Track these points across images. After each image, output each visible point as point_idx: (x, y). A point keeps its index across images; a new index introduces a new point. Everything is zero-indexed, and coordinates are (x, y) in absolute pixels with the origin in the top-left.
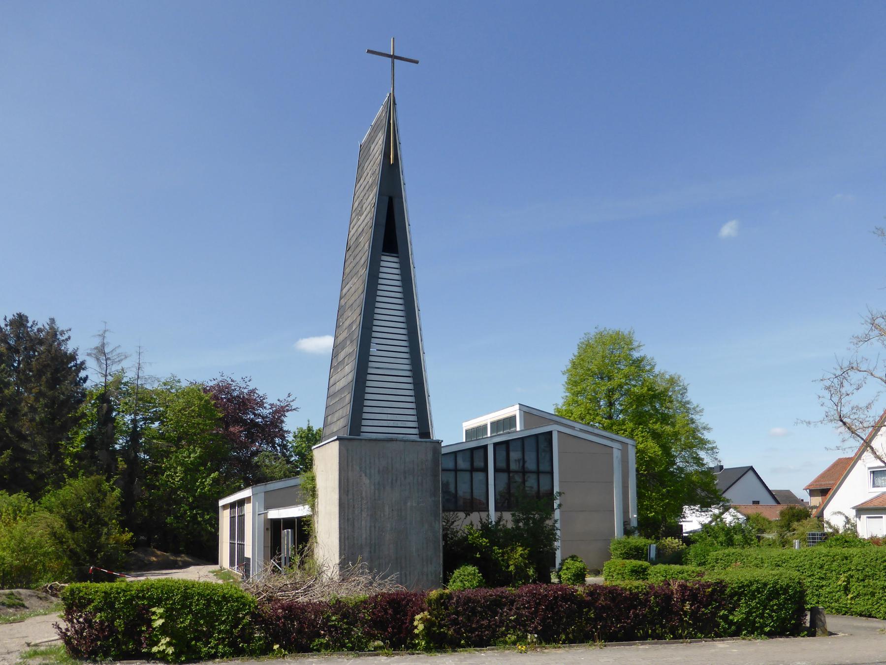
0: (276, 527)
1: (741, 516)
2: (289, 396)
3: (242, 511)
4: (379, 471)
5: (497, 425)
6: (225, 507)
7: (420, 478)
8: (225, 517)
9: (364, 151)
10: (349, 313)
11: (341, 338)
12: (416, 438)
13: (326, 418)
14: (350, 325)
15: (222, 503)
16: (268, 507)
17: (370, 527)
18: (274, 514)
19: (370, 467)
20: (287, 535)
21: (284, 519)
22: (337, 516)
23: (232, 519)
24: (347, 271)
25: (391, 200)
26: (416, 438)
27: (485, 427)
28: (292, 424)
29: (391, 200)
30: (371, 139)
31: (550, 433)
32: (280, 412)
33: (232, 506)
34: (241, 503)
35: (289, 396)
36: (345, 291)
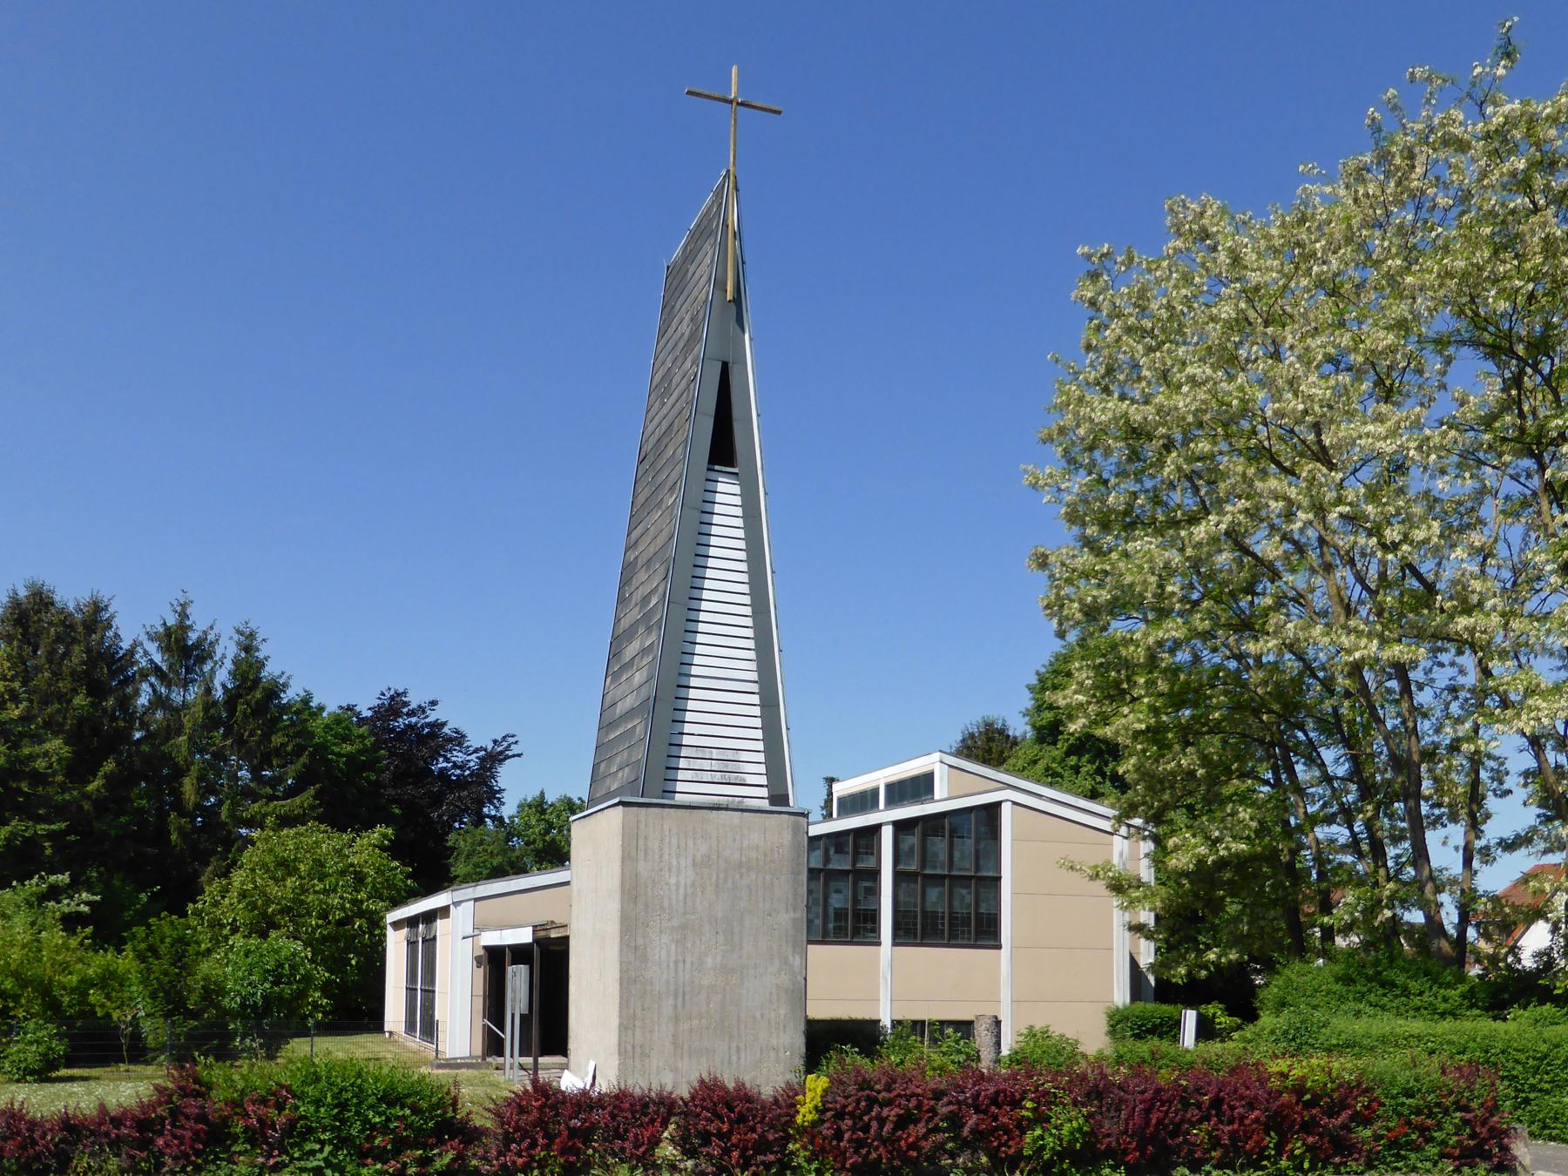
0: (495, 961)
1: (666, 827)
2: (1042, 562)
3: (429, 929)
4: (694, 864)
5: (901, 791)
6: (397, 925)
7: (768, 877)
8: (396, 945)
9: (677, 278)
10: (642, 576)
11: (625, 623)
12: (765, 804)
13: (595, 767)
14: (646, 599)
15: (392, 917)
16: (479, 928)
17: (676, 962)
18: (492, 938)
19: (678, 856)
20: (518, 979)
21: (510, 947)
22: (617, 940)
23: (412, 944)
24: (641, 498)
25: (725, 367)
26: (765, 804)
27: (875, 791)
28: (516, 788)
29: (725, 367)
30: (690, 255)
31: (997, 806)
32: (493, 758)
33: (412, 922)
34: (430, 917)
35: (1042, 562)
36: (634, 535)
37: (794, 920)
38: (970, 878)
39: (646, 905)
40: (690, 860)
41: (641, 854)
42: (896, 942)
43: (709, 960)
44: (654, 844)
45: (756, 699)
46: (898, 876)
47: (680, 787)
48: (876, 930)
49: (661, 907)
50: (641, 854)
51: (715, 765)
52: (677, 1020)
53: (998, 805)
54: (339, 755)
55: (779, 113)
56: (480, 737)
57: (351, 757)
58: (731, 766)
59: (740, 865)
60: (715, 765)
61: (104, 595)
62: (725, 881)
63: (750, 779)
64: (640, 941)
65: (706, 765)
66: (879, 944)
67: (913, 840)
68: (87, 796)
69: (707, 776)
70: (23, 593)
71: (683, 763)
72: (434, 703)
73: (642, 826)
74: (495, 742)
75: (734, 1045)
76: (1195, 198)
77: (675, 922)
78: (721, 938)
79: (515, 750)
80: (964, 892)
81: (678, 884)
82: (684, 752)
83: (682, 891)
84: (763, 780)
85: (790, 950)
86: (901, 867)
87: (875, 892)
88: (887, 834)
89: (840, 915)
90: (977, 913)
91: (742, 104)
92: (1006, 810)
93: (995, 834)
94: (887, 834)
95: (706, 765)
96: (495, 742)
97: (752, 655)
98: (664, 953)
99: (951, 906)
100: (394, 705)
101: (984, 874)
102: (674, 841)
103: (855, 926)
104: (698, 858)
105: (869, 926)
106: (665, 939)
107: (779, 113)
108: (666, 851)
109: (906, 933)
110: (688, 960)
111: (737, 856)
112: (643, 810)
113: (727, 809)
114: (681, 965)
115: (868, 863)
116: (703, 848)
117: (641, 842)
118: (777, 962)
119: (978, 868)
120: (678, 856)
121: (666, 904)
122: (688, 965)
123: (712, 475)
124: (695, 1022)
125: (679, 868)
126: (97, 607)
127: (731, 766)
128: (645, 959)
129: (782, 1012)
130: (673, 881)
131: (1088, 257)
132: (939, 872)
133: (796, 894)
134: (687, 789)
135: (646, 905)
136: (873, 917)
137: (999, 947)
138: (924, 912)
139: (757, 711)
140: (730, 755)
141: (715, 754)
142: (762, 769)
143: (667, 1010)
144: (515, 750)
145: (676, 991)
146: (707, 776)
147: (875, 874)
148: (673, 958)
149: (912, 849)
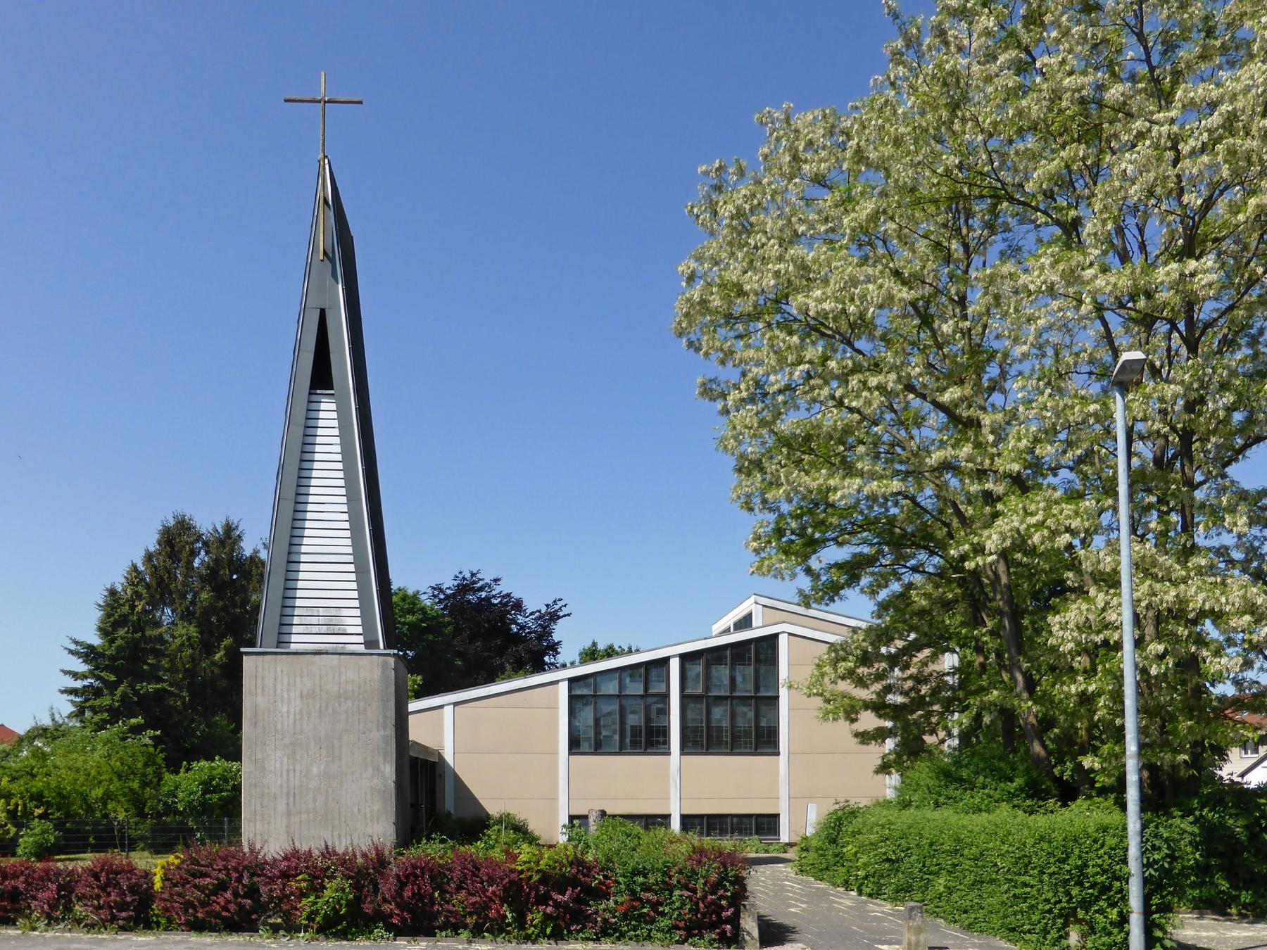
1: (279, 670)
4: (302, 696)
7: (362, 704)
12: (361, 649)
17: (288, 771)
19: (288, 691)
26: (361, 649)
29: (323, 312)
37: (384, 737)
38: (751, 698)
39: (264, 728)
40: (298, 693)
41: (259, 691)
42: (684, 751)
43: (315, 769)
44: (269, 682)
45: (352, 568)
46: (684, 697)
47: (294, 638)
48: (666, 742)
49: (276, 731)
50: (259, 691)
51: (322, 621)
52: (289, 814)
53: (776, 636)
54: (404, 624)
55: (361, 103)
56: (534, 603)
57: (412, 626)
58: (335, 621)
59: (339, 695)
60: (322, 621)
61: (234, 519)
62: (327, 707)
63: (350, 630)
64: (259, 756)
65: (315, 620)
66: (669, 754)
67: (697, 669)
68: (214, 664)
69: (315, 629)
70: (172, 523)
71: (296, 620)
72: (496, 580)
73: (260, 669)
74: (547, 606)
75: (336, 833)
76: (778, 108)
77: (287, 741)
78: (324, 752)
79: (565, 611)
80: (745, 709)
81: (288, 712)
82: (297, 612)
83: (292, 717)
84: (360, 630)
85: (381, 760)
86: (689, 691)
87: (665, 712)
88: (675, 665)
89: (635, 731)
90: (757, 726)
91: (329, 102)
92: (783, 641)
93: (773, 661)
94: (675, 665)
95: (315, 620)
96: (547, 606)
97: (348, 534)
98: (278, 764)
99: (708, 720)
100: (465, 587)
101: (763, 693)
102: (285, 680)
103: (650, 739)
104: (305, 691)
105: (661, 739)
106: (279, 753)
107: (361, 103)
108: (279, 687)
109: (689, 745)
110: (298, 768)
111: (336, 689)
112: (260, 658)
113: (327, 653)
114: (292, 773)
115: (657, 688)
116: (308, 684)
117: (259, 682)
118: (370, 770)
119: (757, 689)
120: (288, 691)
121: (279, 727)
122: (298, 773)
123: (315, 398)
124: (304, 816)
125: (289, 701)
126: (229, 528)
127: (335, 621)
128: (263, 769)
129: (376, 808)
130: (285, 709)
131: (706, 173)
132: (723, 693)
133: (385, 717)
134: (300, 639)
135: (264, 728)
136: (665, 732)
137: (778, 754)
138: (708, 727)
139: (353, 577)
140: (333, 612)
141: (322, 612)
142: (359, 621)
143: (281, 806)
144: (565, 611)
145: (288, 793)
146: (315, 629)
147: (666, 696)
148: (285, 768)
149: (698, 675)
